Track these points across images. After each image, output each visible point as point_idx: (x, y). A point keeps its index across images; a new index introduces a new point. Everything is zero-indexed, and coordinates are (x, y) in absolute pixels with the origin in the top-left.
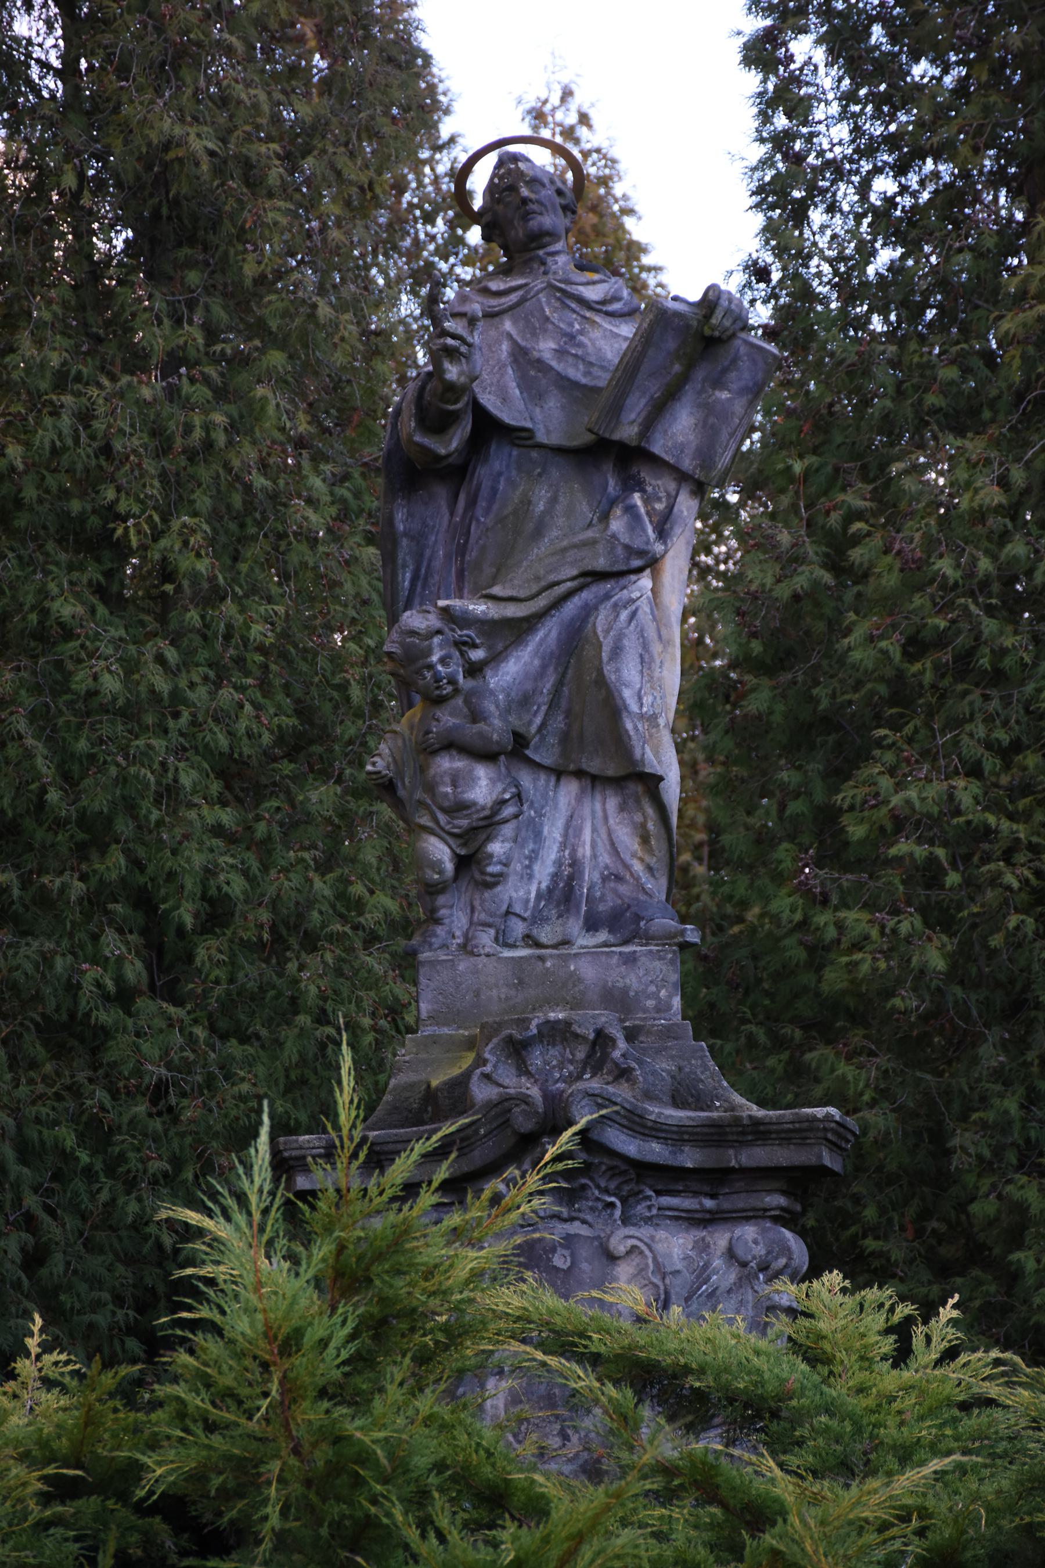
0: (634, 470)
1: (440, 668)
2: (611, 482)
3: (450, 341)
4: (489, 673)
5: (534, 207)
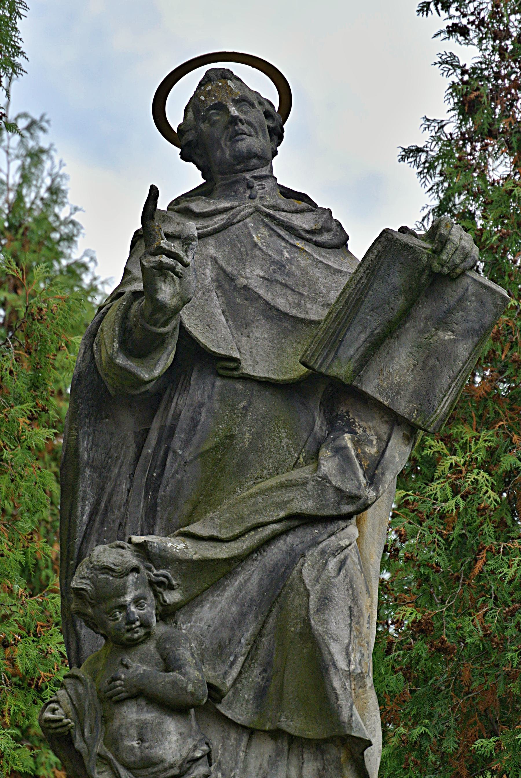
0: (342, 410)
1: (133, 608)
2: (318, 421)
3: (165, 259)
4: (181, 617)
5: (244, 128)
